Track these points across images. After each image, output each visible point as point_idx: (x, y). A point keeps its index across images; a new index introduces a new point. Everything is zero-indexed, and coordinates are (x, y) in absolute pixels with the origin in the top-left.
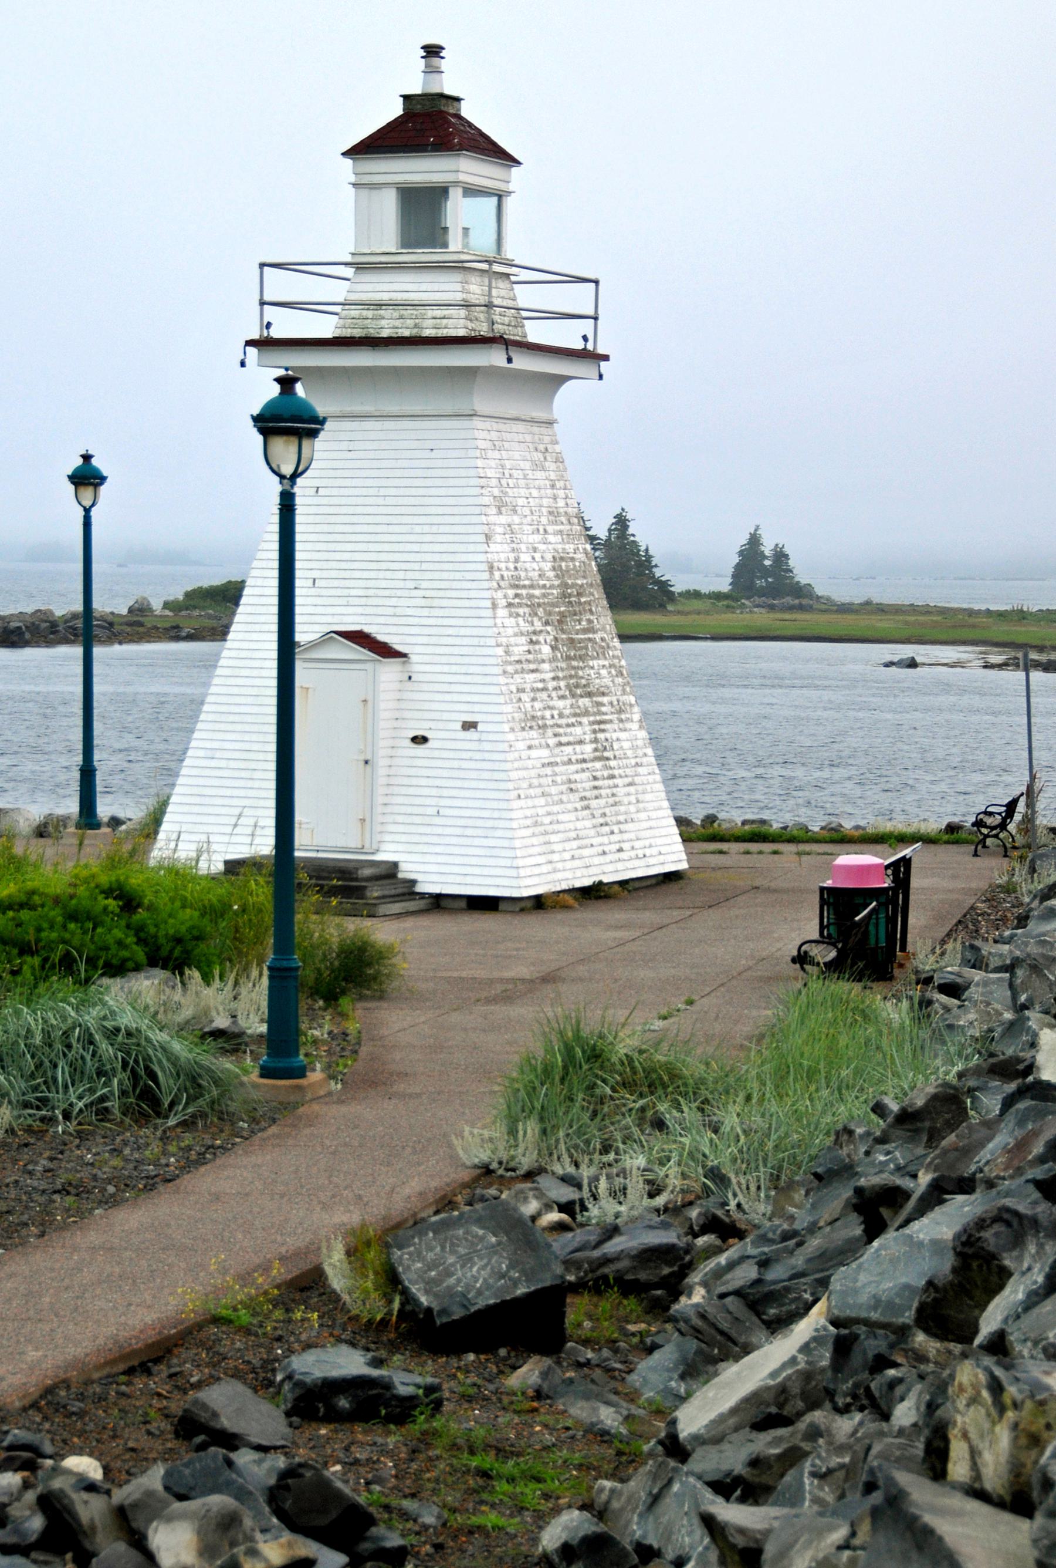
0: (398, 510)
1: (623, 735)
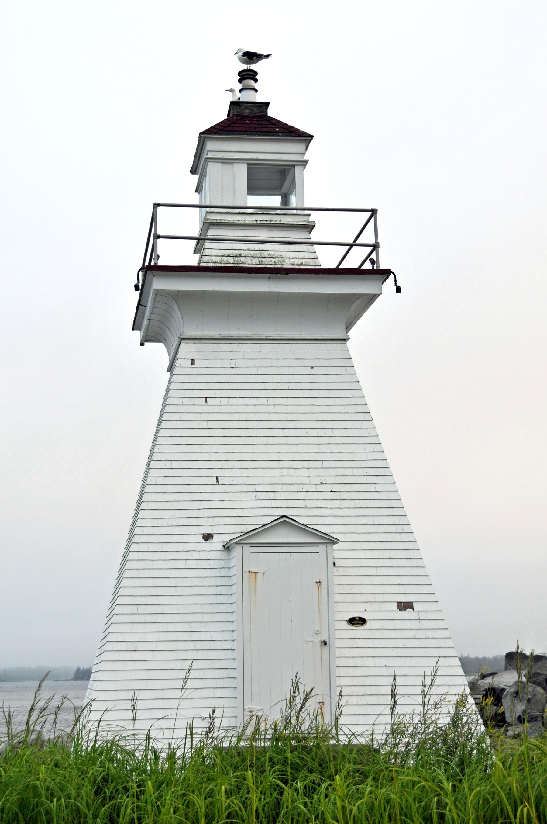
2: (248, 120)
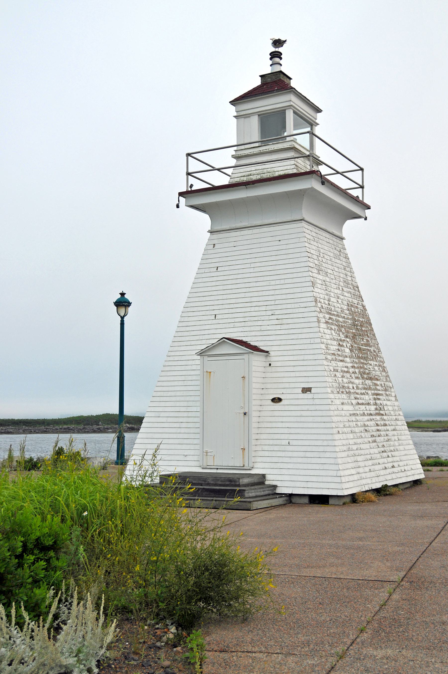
0: (261, 274)
1: (388, 403)
2: (275, 83)
